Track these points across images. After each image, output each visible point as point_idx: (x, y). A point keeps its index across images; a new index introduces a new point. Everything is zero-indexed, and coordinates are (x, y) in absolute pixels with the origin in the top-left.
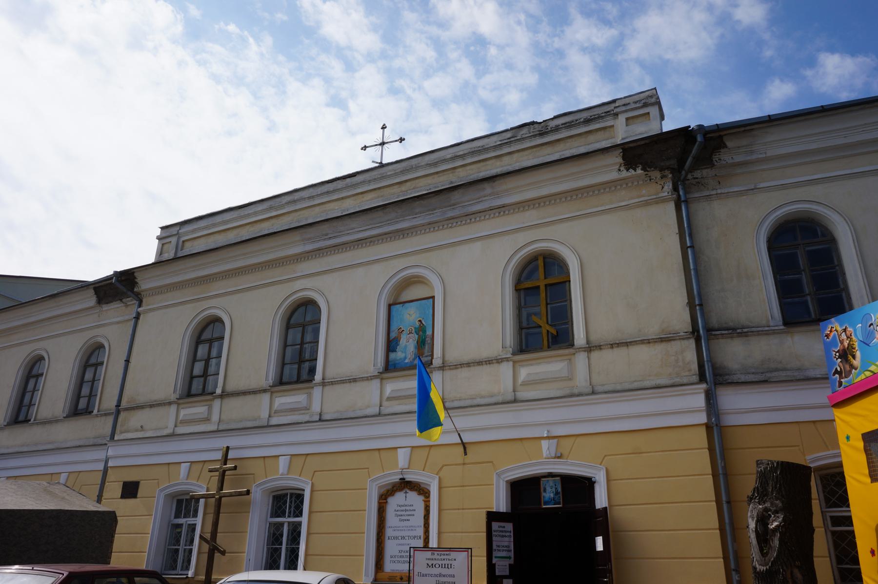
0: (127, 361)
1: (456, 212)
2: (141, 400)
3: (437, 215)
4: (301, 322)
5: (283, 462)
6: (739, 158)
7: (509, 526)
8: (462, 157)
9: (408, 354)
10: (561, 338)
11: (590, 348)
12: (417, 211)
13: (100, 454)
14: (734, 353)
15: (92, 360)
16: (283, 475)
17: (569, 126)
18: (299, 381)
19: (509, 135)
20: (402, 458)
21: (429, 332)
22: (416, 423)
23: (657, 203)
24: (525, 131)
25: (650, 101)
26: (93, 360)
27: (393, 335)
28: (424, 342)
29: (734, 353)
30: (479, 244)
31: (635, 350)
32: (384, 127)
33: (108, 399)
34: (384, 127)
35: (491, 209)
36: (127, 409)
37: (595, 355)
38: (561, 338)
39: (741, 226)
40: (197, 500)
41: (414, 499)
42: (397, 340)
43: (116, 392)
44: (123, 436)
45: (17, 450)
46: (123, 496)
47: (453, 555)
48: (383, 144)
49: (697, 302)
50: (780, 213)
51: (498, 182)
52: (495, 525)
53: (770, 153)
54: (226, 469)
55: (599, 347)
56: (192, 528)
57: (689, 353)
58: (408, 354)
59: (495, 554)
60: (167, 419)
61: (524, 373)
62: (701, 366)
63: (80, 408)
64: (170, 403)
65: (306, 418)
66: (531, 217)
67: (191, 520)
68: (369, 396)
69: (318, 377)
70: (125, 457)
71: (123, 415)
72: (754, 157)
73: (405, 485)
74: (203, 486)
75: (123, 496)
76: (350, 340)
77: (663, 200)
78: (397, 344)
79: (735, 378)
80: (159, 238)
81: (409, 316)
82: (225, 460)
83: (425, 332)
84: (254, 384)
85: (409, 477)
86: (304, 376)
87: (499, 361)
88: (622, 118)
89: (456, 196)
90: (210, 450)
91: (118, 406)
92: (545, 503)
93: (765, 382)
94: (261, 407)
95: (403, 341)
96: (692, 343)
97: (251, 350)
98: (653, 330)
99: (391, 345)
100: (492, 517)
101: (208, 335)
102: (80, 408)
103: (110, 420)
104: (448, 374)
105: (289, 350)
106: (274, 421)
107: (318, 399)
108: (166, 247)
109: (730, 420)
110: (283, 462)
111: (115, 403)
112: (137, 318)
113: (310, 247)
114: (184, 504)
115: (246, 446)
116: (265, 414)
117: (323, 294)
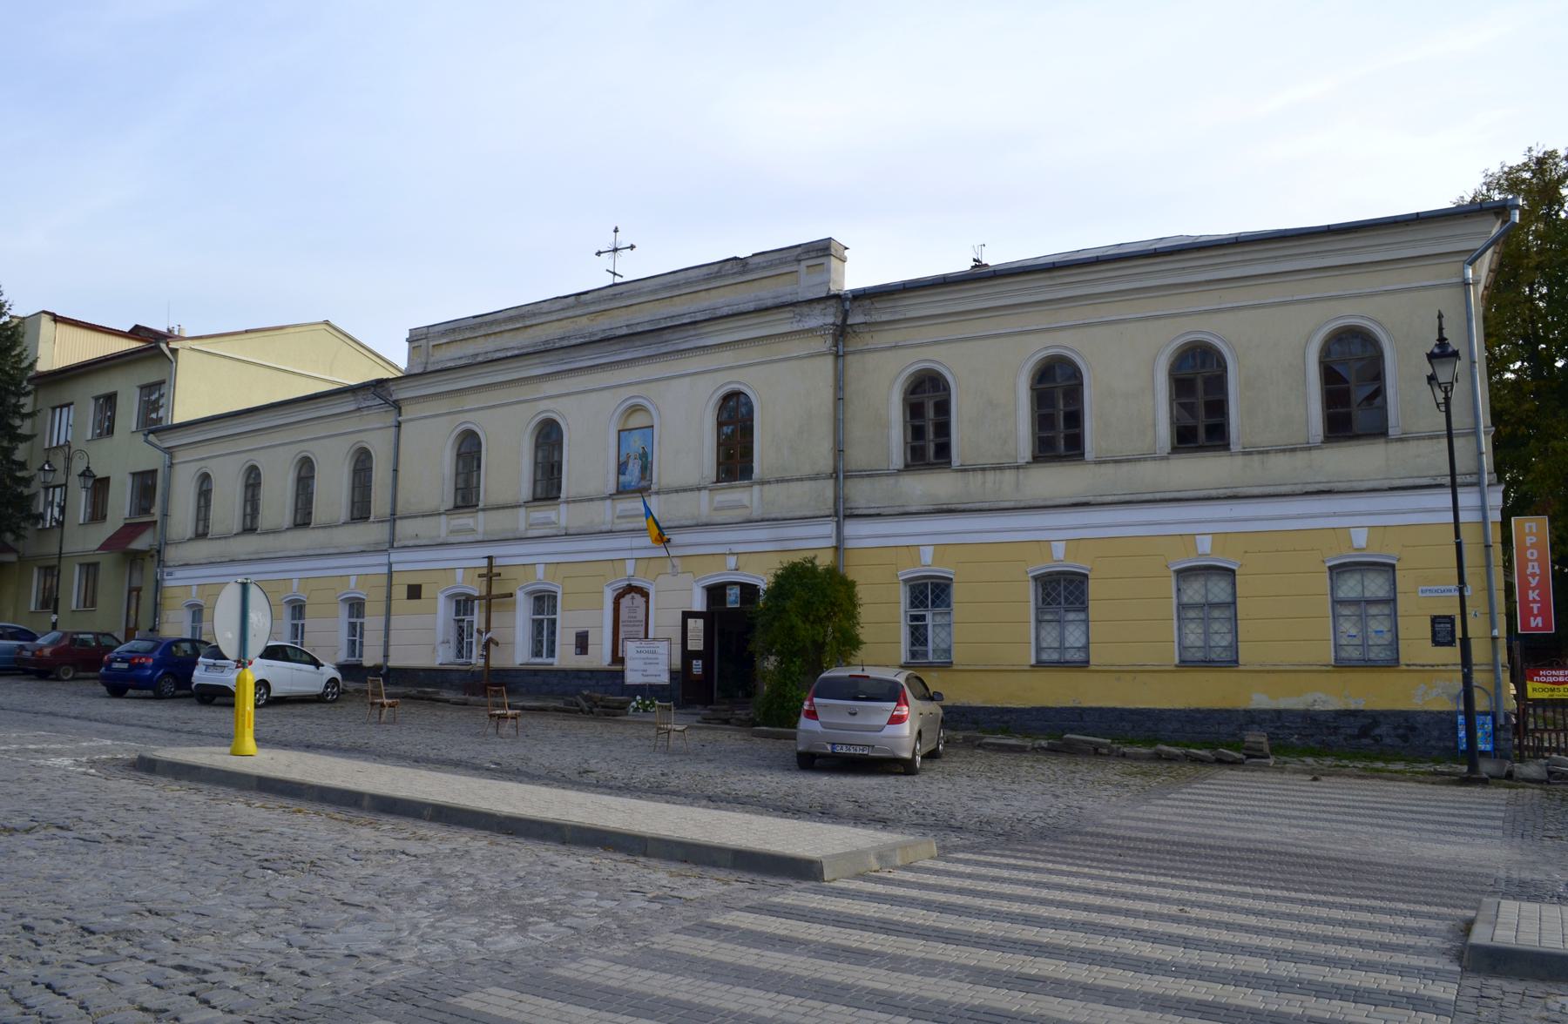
0: (396, 471)
3: (1239, 258)
4: (549, 436)
6: (885, 318)
7: (700, 623)
9: (635, 477)
10: (1073, 448)
11: (762, 483)
13: (383, 559)
14: (862, 494)
15: (362, 463)
16: (541, 578)
17: (771, 265)
19: (716, 268)
24: (729, 265)
25: (822, 251)
28: (646, 468)
29: (862, 494)
30: (687, 379)
31: (793, 485)
32: (616, 231)
33: (380, 502)
34: (616, 231)
38: (1073, 448)
41: (639, 600)
46: (409, 597)
48: (616, 250)
49: (839, 451)
51: (751, 306)
52: (691, 622)
53: (909, 315)
56: (471, 623)
57: (828, 487)
58: (635, 477)
60: (442, 527)
65: (554, 532)
66: (727, 358)
67: (468, 618)
68: (603, 514)
70: (408, 564)
71: (399, 523)
73: (630, 589)
74: (476, 588)
75: (409, 597)
76: (588, 462)
81: (635, 443)
82: (490, 566)
85: (634, 583)
86: (1375, 586)
88: (804, 264)
89: (667, 335)
90: (475, 558)
91: (393, 514)
93: (879, 515)
94: (521, 520)
96: (831, 482)
97: (508, 467)
98: (807, 470)
99: (622, 468)
100: (687, 615)
101: (469, 450)
102: (360, 511)
107: (560, 515)
111: (388, 511)
112: (399, 425)
114: (463, 604)
115: (507, 555)
116: (522, 526)
117: (564, 417)
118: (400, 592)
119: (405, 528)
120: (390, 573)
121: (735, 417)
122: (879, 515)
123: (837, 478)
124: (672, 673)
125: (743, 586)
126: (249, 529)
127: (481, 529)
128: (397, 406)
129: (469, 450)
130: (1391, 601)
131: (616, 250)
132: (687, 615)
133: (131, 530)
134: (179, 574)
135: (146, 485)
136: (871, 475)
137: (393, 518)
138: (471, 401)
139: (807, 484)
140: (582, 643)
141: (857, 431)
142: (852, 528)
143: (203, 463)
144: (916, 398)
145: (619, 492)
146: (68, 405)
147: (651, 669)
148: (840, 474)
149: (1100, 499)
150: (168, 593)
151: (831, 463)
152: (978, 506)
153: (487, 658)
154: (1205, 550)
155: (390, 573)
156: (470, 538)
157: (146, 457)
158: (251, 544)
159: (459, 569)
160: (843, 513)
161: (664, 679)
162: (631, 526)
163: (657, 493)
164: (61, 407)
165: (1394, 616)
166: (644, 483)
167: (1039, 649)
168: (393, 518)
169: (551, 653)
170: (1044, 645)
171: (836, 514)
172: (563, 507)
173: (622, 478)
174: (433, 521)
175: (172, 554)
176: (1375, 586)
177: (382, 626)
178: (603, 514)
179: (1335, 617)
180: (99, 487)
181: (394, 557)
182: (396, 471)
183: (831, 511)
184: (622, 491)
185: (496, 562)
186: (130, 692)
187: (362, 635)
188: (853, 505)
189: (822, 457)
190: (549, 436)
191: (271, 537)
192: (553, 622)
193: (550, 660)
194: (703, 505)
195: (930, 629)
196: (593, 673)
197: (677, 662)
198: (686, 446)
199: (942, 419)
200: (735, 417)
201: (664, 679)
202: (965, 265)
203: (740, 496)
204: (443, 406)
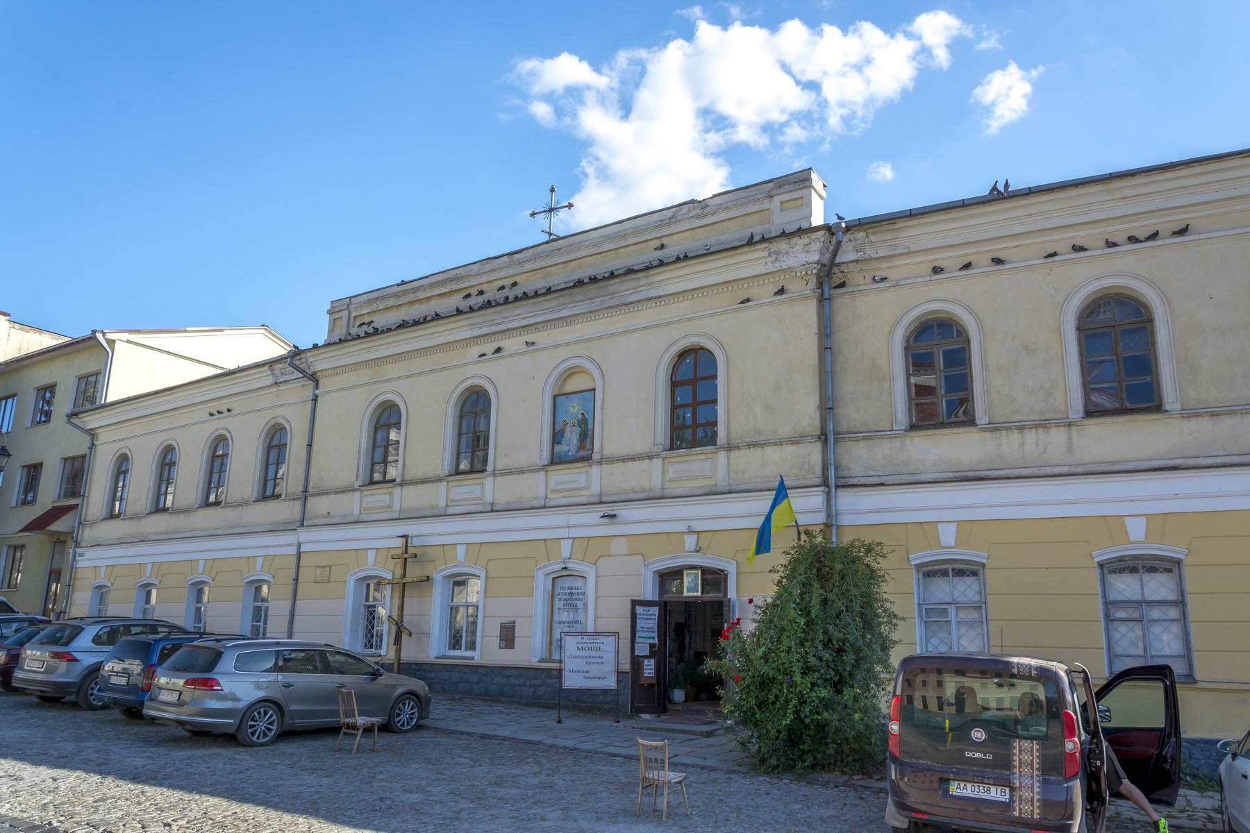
0: (310, 446)
1: (616, 302)
2: (327, 485)
4: (474, 406)
5: (461, 551)
8: (624, 236)
9: (573, 441)
11: (729, 448)
12: (578, 299)
13: (291, 538)
14: (857, 458)
15: (275, 445)
18: (471, 471)
19: (669, 213)
20: (565, 548)
21: (590, 426)
22: (548, 62)
23: (800, 300)
24: (685, 208)
26: (275, 442)
27: (558, 428)
28: (586, 436)
29: (857, 458)
31: (770, 450)
33: (291, 473)
34: (552, 190)
35: (648, 299)
36: (313, 495)
37: (734, 454)
39: (878, 325)
40: (1006, 783)
42: (562, 432)
43: (302, 475)
44: (311, 523)
45: (212, 532)
47: (602, 639)
49: (827, 407)
50: (916, 313)
52: (639, 610)
54: (408, 554)
55: (738, 448)
57: (814, 453)
58: (573, 441)
59: (638, 634)
60: (351, 504)
61: (672, 470)
62: (825, 468)
63: (268, 493)
64: (354, 490)
65: (479, 508)
69: (490, 468)
71: (310, 500)
72: (898, 252)
76: (519, 429)
77: (807, 297)
78: (562, 437)
79: (855, 481)
80: (329, 312)
81: (573, 409)
83: (587, 425)
84: (431, 472)
86: (478, 466)
87: (650, 457)
88: (778, 199)
89: (614, 285)
90: (387, 536)
91: (305, 491)
92: (1111, 361)
93: (882, 484)
94: (437, 495)
95: (567, 434)
96: (819, 446)
97: (427, 439)
98: (786, 431)
99: (557, 437)
102: (268, 493)
103: (298, 504)
104: (606, 467)
105: (464, 438)
106: (451, 511)
107: (489, 488)
108: (338, 323)
109: (845, 520)
110: (461, 551)
111: (301, 488)
113: (478, 332)
114: (369, 584)
115: (428, 532)
118: (607, 509)
119: (319, 505)
120: (299, 554)
121: (693, 377)
122: (882, 484)
123: (825, 442)
124: (619, 673)
125: (705, 571)
126: (159, 509)
127: (396, 506)
128: (314, 378)
129: (387, 417)
130: (1181, 603)
131: (551, 210)
132: (635, 603)
133: (56, 513)
134: (90, 554)
135: (76, 474)
136: (869, 435)
137: (305, 494)
138: (392, 370)
139: (789, 450)
140: (508, 635)
141: (849, 385)
142: (846, 501)
143: (122, 444)
144: (921, 348)
145: (552, 463)
146: (13, 396)
147: (595, 670)
148: (828, 434)
149: (1193, 462)
150: (80, 574)
151: (817, 423)
152: (1017, 472)
153: (398, 652)
154: (1137, 538)
155: (299, 554)
156: (385, 516)
157: (76, 445)
158: (160, 523)
159: (373, 545)
160: (833, 480)
161: (611, 683)
162: (569, 501)
163: (600, 463)
164: (6, 398)
165: (1184, 619)
166: (582, 453)
167: (1112, 657)
168: (305, 494)
169: (472, 646)
170: (1118, 651)
171: (825, 483)
172: (489, 481)
173: (557, 448)
174: (346, 498)
175: (88, 534)
176: (1159, 587)
177: (298, 603)
178: (532, 487)
179: (1109, 619)
180: (34, 471)
181: (304, 535)
182: (310, 446)
183: (818, 481)
184: (556, 460)
185: (304, 548)
186: (482, 427)
187: (265, 623)
188: (845, 473)
189: (807, 414)
190: (474, 406)
191: (182, 517)
192: (267, 609)
193: (469, 654)
194: (651, 474)
195: (953, 624)
196: (521, 671)
197: (626, 666)
198: (633, 412)
199: (956, 371)
200: (693, 377)
201: (611, 683)
202: (985, 191)
203: (697, 466)
204: (363, 376)
